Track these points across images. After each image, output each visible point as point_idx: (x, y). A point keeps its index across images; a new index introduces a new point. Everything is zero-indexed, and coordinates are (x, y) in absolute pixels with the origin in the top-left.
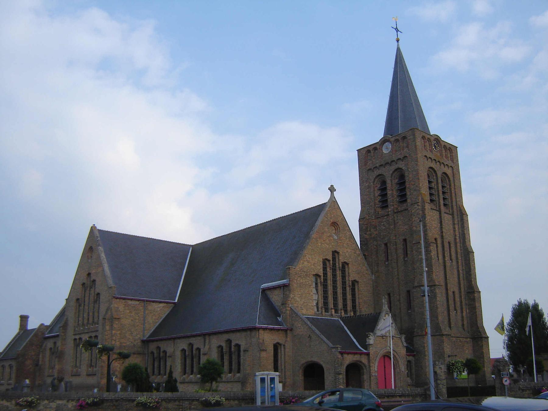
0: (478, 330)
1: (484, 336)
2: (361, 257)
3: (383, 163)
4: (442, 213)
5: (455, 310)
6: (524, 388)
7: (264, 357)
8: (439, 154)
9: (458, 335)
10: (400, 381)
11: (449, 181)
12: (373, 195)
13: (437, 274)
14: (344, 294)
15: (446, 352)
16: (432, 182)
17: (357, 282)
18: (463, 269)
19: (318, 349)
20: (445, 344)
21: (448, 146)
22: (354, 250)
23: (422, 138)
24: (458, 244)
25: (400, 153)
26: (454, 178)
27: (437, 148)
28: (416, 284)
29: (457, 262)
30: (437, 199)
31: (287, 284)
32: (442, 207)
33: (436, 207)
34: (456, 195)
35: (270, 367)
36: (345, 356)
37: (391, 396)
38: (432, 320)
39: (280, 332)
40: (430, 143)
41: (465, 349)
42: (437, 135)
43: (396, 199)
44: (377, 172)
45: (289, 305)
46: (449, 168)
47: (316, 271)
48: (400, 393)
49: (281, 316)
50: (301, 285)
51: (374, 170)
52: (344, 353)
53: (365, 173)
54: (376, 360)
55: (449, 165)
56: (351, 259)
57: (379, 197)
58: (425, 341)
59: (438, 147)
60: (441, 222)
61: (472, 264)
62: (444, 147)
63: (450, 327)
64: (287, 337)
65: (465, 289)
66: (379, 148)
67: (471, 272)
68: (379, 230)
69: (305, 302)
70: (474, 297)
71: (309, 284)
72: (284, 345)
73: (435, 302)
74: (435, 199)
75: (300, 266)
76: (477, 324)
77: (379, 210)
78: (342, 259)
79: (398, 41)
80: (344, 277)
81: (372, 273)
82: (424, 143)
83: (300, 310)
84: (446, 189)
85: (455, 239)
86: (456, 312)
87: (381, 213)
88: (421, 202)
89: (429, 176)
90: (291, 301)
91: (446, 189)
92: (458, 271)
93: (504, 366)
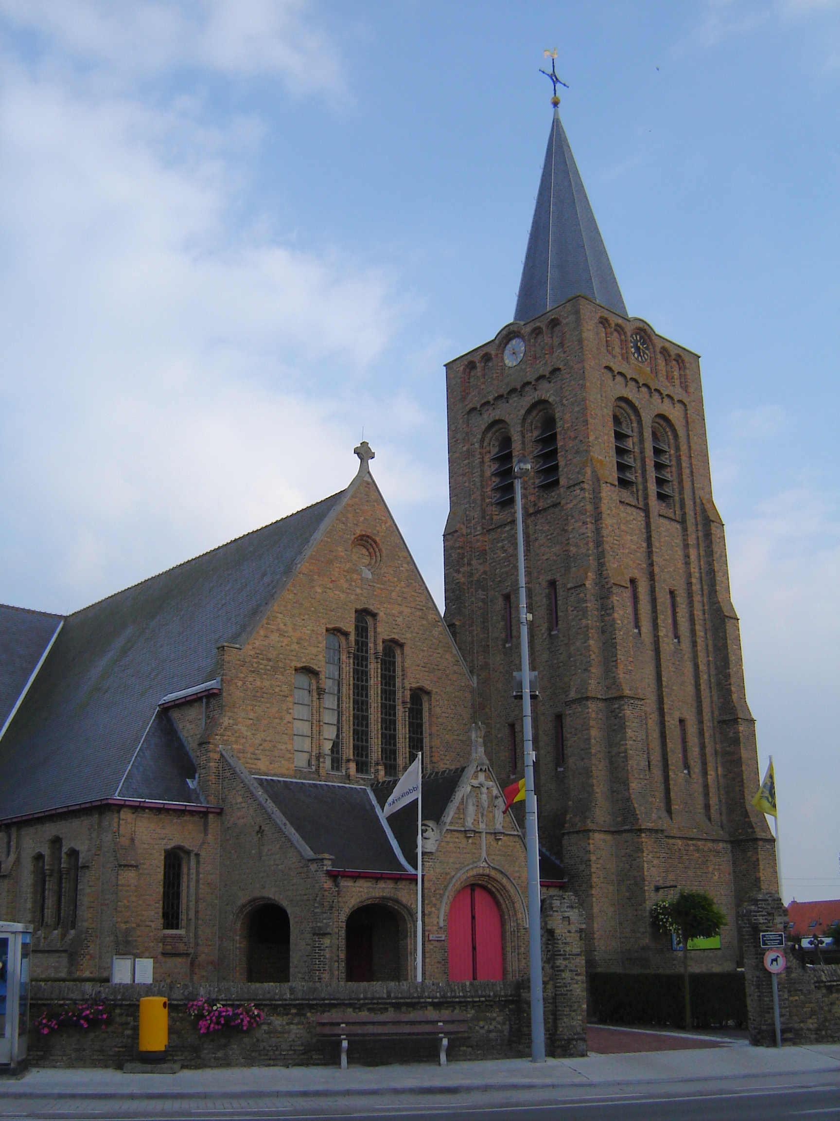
0: (747, 820)
1: (761, 835)
2: (440, 629)
3: (504, 391)
4: (651, 515)
5: (687, 766)
6: (834, 981)
7: (129, 886)
8: (649, 369)
9: (694, 833)
10: (518, 954)
11: (676, 436)
12: (479, 473)
13: (630, 668)
14: (389, 724)
15: (648, 878)
16: (629, 436)
17: (428, 693)
18: (709, 661)
19: (277, 865)
20: (647, 856)
21: (673, 352)
22: (422, 610)
23: (601, 323)
24: (697, 598)
25: (544, 361)
26: (688, 430)
27: (644, 353)
28: (573, 695)
29: (694, 644)
30: (640, 480)
31: (215, 691)
32: (653, 501)
33: (638, 499)
34: (692, 472)
35: (153, 913)
36: (345, 883)
37: (408, 1005)
38: (614, 792)
39: (187, 818)
40: (623, 337)
41: (710, 869)
42: (640, 320)
43: (532, 481)
44: (490, 414)
45: (217, 746)
46: (674, 404)
47: (304, 660)
48: (438, 994)
49: (197, 776)
50: (258, 694)
51: (483, 412)
52: (343, 877)
53: (461, 421)
54: (442, 896)
55: (676, 398)
56: (412, 632)
57: (494, 479)
58: (591, 846)
59: (647, 352)
60: (649, 539)
61: (731, 647)
62: (661, 352)
63: (669, 811)
64: (206, 831)
65: (712, 713)
66: (497, 355)
67: (729, 669)
68: (491, 561)
69: (268, 739)
70: (737, 733)
71: (282, 693)
72: (197, 855)
73: (622, 742)
74: (634, 478)
75: (257, 643)
76: (743, 806)
77: (495, 510)
78: (383, 631)
79: (556, 104)
80: (388, 679)
81: (471, 672)
82: (606, 337)
83: (250, 761)
84: (666, 458)
85: (690, 584)
86: (689, 772)
87: (498, 517)
88: (590, 482)
89: (617, 420)
90: (222, 735)
91: (667, 456)
92: (696, 666)
93: (769, 914)
